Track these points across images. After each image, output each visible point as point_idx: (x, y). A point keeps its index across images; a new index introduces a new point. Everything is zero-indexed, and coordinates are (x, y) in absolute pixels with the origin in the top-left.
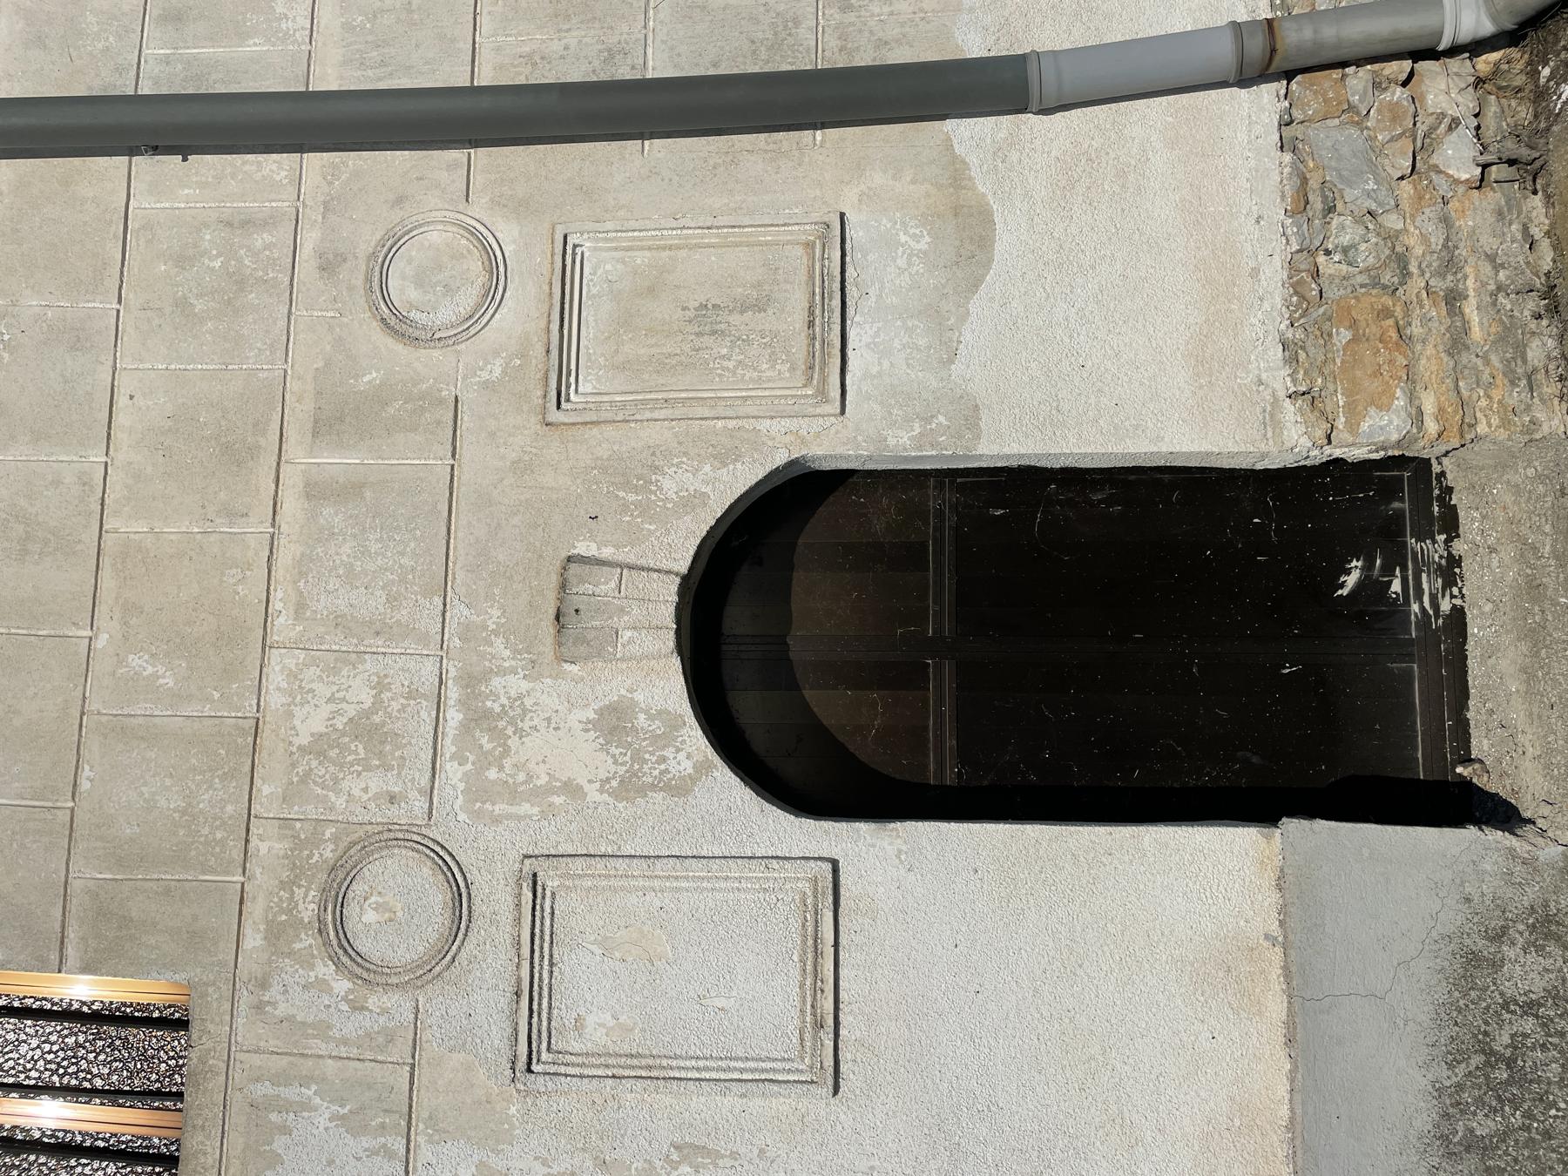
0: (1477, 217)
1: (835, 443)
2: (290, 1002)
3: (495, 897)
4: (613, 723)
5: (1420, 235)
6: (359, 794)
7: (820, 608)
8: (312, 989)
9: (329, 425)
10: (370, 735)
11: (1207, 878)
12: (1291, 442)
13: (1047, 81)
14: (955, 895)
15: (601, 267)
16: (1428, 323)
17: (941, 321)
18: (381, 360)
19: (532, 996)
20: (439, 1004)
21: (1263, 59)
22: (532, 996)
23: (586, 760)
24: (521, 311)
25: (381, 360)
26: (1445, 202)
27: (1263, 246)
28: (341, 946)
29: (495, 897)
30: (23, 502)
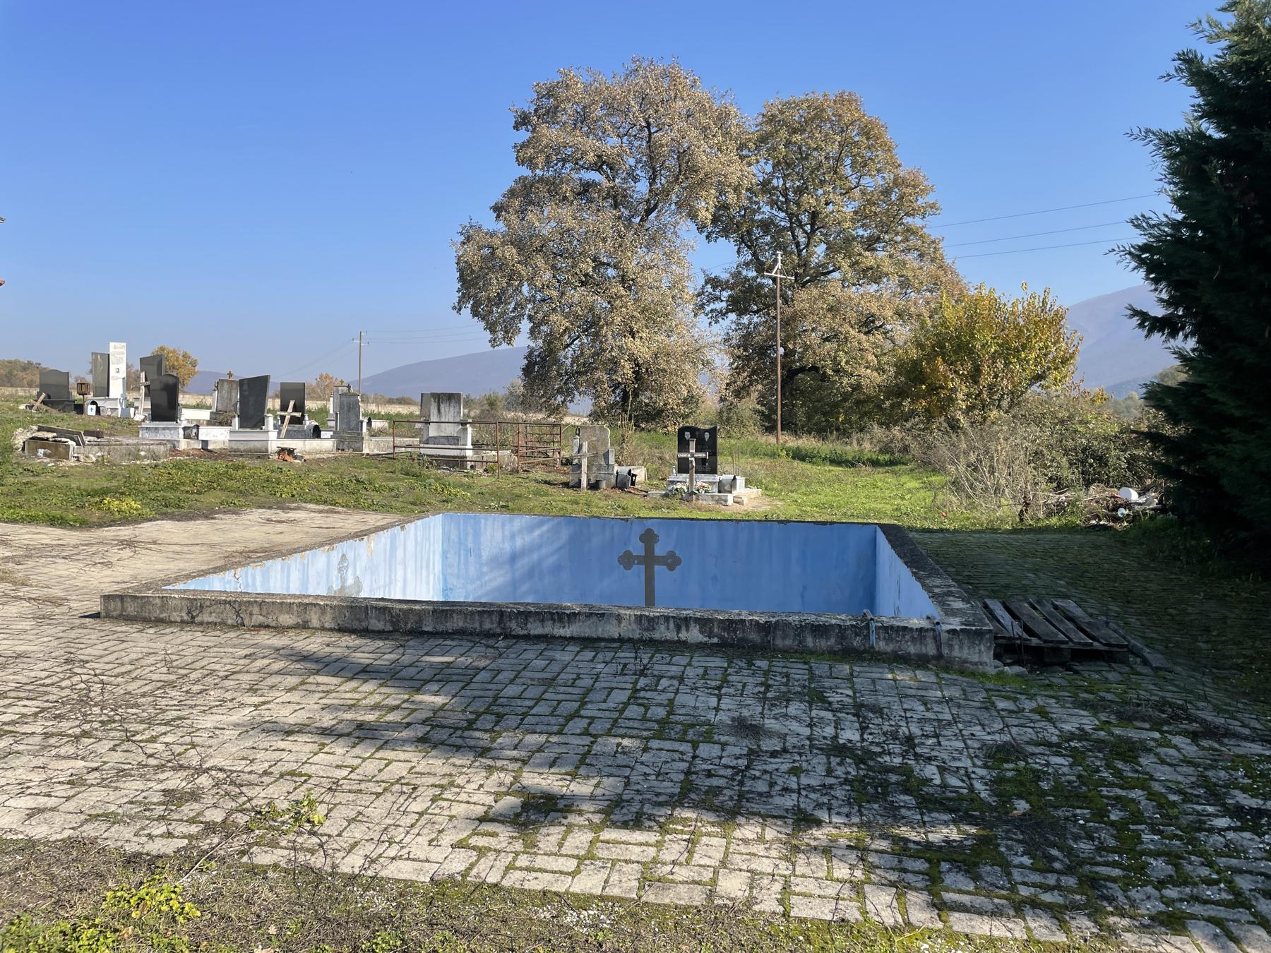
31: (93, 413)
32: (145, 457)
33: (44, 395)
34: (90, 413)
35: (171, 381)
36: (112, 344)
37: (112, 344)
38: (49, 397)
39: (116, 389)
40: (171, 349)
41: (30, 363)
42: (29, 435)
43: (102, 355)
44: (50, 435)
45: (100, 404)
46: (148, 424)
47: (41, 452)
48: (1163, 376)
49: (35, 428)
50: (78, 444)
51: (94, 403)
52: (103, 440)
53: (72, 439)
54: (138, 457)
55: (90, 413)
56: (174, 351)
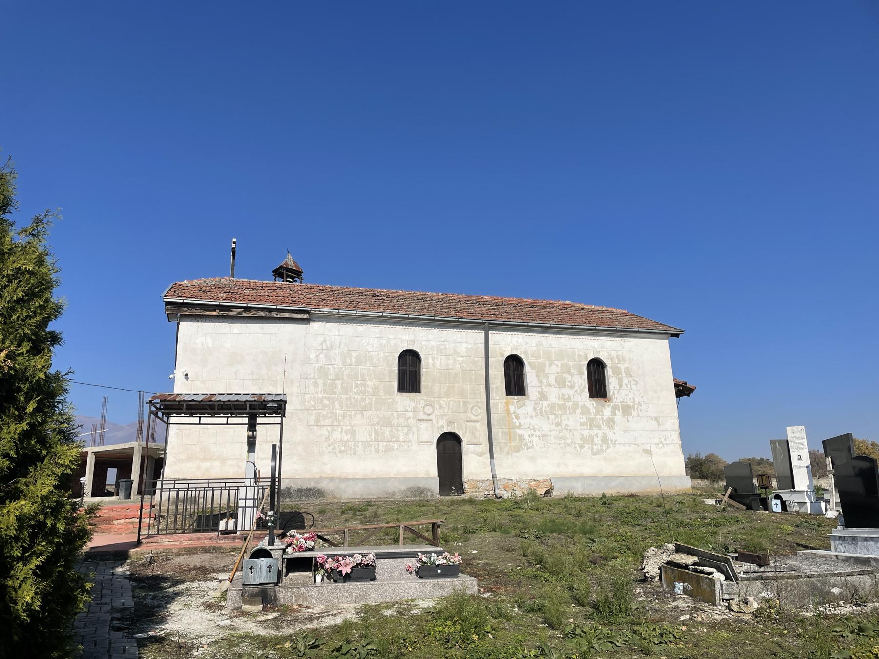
0: (482, 494)
1: (464, 444)
2: (422, 402)
3: (430, 417)
4: (443, 426)
5: (481, 489)
6: (437, 406)
7: (450, 443)
8: (422, 403)
9: (465, 403)
10: (441, 407)
11: (434, 471)
12: (465, 479)
13: (852, 561)
14: (431, 453)
15: (477, 425)
16: (474, 490)
17: (474, 452)
18: (470, 406)
19: (423, 420)
20: (421, 414)
21: (494, 477)
22: (423, 420)
23: (440, 424)
24: (474, 418)
25: (470, 406)
26: (629, 549)
27: (480, 478)
28: (425, 406)
29: (430, 417)
30: (553, 371)
31: (779, 509)
32: (840, 597)
33: (730, 489)
34: (774, 509)
35: (865, 465)
36: (789, 429)
37: (789, 429)
38: (735, 490)
39: (802, 480)
40: (861, 440)
41: (762, 460)
42: (665, 558)
43: (780, 442)
44: (689, 560)
45: (785, 497)
46: (839, 531)
47: (679, 586)
48: (209, 485)
49: (671, 546)
50: (728, 578)
51: (778, 497)
52: (767, 572)
53: (720, 570)
54: (826, 598)
55: (774, 509)
56: (863, 442)
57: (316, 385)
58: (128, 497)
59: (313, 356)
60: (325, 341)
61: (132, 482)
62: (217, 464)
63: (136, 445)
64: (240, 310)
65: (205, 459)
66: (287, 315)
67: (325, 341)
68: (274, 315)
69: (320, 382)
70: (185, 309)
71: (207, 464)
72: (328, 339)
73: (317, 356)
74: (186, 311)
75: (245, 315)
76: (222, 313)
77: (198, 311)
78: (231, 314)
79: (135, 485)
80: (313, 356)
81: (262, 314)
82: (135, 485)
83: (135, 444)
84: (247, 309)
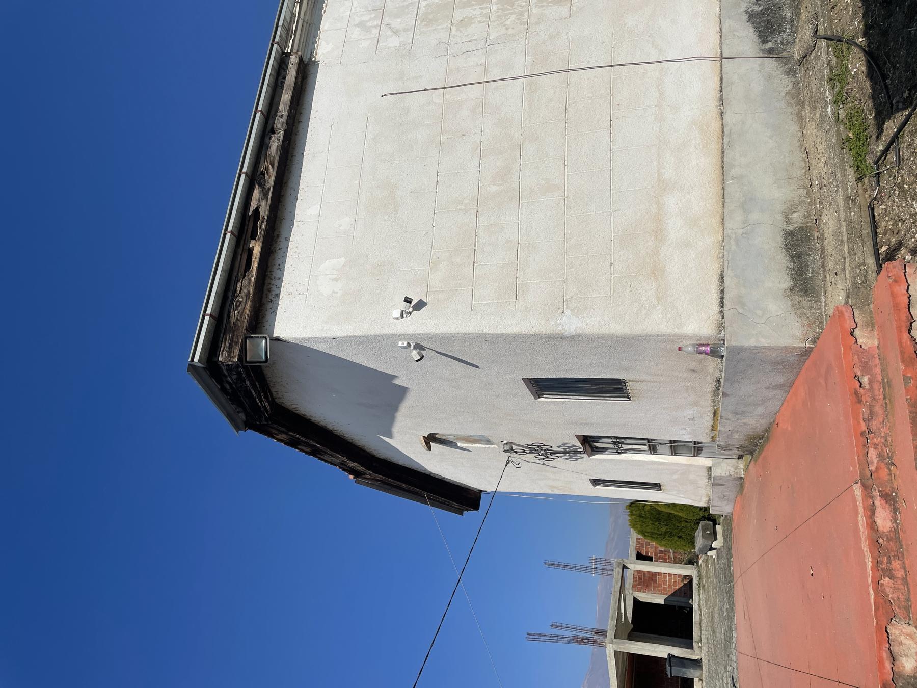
57: (464, 23)
58: (697, 664)
59: (394, 42)
60: (361, 25)
61: (671, 656)
62: (672, 202)
63: (611, 647)
64: (256, 194)
65: (659, 234)
66: (286, 96)
67: (361, 25)
68: (280, 122)
69: (458, 15)
70: (235, 315)
71: (675, 228)
72: (357, 20)
73: (396, 32)
74: (242, 312)
75: (271, 182)
76: (263, 234)
77: (247, 285)
78: (264, 211)
79: (677, 652)
80: (394, 42)
81: (275, 144)
82: (677, 652)
83: (610, 649)
84: (255, 178)
